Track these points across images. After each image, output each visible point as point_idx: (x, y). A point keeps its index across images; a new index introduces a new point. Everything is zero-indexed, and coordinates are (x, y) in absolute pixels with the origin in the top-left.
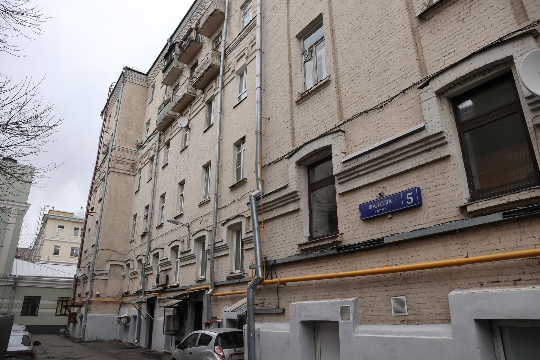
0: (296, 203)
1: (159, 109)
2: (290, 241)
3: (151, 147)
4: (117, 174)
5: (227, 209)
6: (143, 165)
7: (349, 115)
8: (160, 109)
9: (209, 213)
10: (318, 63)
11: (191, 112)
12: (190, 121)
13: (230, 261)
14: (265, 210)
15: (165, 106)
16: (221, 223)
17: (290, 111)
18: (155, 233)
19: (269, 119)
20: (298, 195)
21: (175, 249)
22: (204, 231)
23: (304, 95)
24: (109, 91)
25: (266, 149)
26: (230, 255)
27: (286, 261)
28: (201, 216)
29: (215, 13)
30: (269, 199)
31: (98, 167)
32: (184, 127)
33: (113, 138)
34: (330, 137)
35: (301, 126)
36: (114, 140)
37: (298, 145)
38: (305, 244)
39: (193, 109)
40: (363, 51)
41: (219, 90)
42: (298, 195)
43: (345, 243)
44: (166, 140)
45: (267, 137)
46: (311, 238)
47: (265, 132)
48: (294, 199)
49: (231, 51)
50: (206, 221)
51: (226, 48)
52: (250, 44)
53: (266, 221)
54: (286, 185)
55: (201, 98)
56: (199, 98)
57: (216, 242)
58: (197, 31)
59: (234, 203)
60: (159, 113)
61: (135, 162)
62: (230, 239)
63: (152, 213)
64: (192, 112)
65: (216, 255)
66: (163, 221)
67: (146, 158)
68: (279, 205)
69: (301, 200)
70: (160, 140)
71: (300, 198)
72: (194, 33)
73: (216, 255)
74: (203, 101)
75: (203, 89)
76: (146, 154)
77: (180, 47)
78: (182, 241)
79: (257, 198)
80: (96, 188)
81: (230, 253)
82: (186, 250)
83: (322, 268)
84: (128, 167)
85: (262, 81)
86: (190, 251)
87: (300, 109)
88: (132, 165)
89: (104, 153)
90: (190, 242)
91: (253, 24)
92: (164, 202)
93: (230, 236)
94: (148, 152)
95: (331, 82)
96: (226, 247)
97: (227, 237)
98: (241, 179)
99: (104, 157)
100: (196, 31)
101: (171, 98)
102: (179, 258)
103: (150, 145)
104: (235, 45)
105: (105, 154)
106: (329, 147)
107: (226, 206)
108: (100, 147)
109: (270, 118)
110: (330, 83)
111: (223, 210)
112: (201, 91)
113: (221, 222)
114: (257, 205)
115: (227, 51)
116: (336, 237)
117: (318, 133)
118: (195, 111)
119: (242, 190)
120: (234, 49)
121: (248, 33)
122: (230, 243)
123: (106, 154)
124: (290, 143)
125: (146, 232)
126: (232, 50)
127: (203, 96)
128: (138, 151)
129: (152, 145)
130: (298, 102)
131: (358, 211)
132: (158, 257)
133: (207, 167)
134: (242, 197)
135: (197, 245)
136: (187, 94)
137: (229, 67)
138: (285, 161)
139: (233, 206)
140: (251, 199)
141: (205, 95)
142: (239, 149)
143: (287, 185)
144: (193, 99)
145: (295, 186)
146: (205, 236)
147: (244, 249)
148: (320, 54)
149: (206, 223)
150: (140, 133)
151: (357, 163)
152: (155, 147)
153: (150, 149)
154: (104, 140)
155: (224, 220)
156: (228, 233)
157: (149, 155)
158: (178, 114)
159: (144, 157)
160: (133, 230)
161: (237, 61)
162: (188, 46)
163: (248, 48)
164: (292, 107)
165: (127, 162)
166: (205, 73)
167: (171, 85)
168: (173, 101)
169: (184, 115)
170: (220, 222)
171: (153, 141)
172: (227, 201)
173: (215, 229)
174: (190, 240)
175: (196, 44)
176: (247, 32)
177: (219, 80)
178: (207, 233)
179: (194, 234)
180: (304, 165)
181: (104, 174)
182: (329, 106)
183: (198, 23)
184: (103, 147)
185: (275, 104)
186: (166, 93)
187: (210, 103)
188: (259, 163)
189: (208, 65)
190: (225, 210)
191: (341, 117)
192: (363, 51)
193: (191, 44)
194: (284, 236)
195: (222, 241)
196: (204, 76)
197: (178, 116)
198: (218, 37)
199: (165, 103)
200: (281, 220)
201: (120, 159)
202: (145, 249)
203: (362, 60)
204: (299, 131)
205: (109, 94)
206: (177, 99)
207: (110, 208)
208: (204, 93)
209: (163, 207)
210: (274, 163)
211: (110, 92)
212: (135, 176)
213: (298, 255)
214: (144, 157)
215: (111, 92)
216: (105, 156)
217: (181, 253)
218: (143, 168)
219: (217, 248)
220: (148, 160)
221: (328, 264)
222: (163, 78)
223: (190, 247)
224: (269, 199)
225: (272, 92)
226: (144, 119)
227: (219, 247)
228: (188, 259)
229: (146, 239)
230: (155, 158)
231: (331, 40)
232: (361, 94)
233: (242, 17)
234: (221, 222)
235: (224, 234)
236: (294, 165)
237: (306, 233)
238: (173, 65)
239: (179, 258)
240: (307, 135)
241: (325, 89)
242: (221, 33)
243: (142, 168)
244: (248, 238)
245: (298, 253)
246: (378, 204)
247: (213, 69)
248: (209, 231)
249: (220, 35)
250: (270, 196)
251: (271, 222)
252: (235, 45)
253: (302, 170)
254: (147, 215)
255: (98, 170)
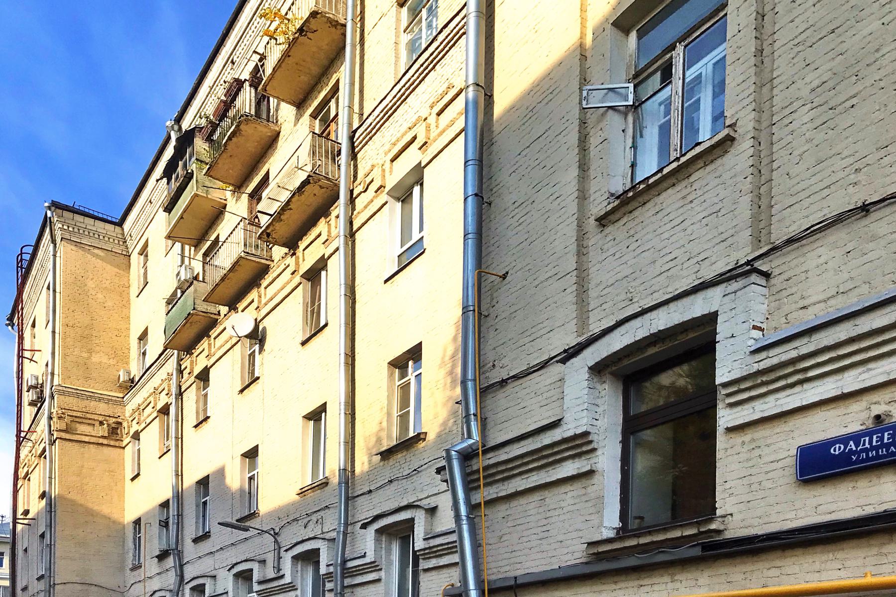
0: (583, 458)
1: (168, 303)
2: (560, 538)
3: (159, 387)
4: (76, 445)
5: (373, 496)
6: (143, 425)
7: (791, 229)
8: (171, 301)
9: (327, 506)
10: (688, 104)
11: (260, 302)
12: (260, 322)
13: (383, 591)
14: (489, 480)
15: (183, 293)
16: (360, 524)
17: (576, 247)
18: (190, 550)
19: (504, 277)
20: (591, 442)
21: (243, 575)
22: (316, 540)
23: (631, 194)
24: (18, 267)
25: (494, 349)
26: (383, 581)
27: (544, 578)
28: (307, 514)
29: (313, 24)
30: (503, 455)
31: (24, 431)
32: (246, 336)
33: (50, 371)
34: (718, 291)
35: (611, 281)
36: (53, 374)
37: (596, 328)
38: (609, 541)
39: (265, 294)
40: (885, 20)
41: (340, 242)
42: (591, 442)
43: (732, 533)
44: (197, 370)
45: (496, 321)
46: (623, 532)
47: (492, 310)
48: (579, 450)
49: (370, 136)
50: (319, 522)
51: (354, 128)
52: (432, 107)
53: (490, 503)
54: (555, 421)
55: (289, 266)
56: (282, 267)
57: (348, 558)
58: (256, 89)
59: (392, 485)
60: (170, 310)
61: (120, 420)
62: (383, 552)
63: (178, 515)
64: (264, 301)
65: (347, 582)
66: (209, 529)
67: (149, 410)
68: (531, 466)
69: (599, 452)
70: (180, 372)
71: (596, 447)
72: (246, 100)
73: (347, 582)
74: (293, 273)
75: (292, 245)
76: (148, 402)
77: (209, 139)
78: (260, 562)
79: (467, 456)
80: (27, 474)
81: (383, 577)
82: (271, 574)
83: (656, 587)
84: (103, 431)
85: (484, 180)
86: (282, 576)
87: (610, 237)
88: (114, 425)
89: (32, 404)
90: (281, 563)
91: (441, 43)
92: (206, 494)
93: (384, 546)
94: (151, 399)
95: (736, 142)
96: (373, 567)
97: (375, 547)
98: (411, 434)
99: (36, 411)
100: (253, 91)
101: (198, 274)
102: (254, 590)
103: (156, 382)
104: (384, 115)
105: (36, 405)
106: (711, 319)
107: (370, 491)
108: (20, 392)
109: (507, 273)
110: (731, 146)
111: (360, 500)
112: (286, 250)
113: (360, 521)
114: (465, 470)
115: (357, 135)
116: (711, 520)
117: (670, 289)
118: (271, 299)
119: (413, 458)
120: (379, 128)
121: (427, 74)
122: (383, 560)
123: (39, 405)
124: (572, 326)
125: (170, 550)
126: (375, 133)
127: (290, 261)
128: (125, 399)
129: (160, 382)
130: (603, 221)
131: (791, 461)
132: (203, 592)
133: (316, 415)
134: (415, 470)
135: (299, 566)
136: (243, 258)
137: (368, 180)
138: (556, 369)
139: (391, 489)
140: (449, 458)
141: (298, 258)
142: (403, 375)
143: (560, 420)
144: (264, 270)
145: (585, 421)
146: (319, 549)
147: (420, 568)
148: (696, 74)
149: (320, 526)
150: (125, 360)
151: (806, 346)
152: (169, 386)
153: (156, 392)
154: (27, 375)
155: (369, 518)
156: (377, 541)
157: (156, 404)
158: (224, 310)
159: (143, 410)
160: (136, 548)
161: (392, 161)
162: (234, 134)
163: (426, 119)
164: (581, 236)
165: (98, 420)
166: (293, 200)
167: (197, 245)
168: (207, 279)
169: (243, 311)
170: (356, 522)
171: (162, 374)
172: (374, 482)
173: (343, 535)
174: (281, 560)
175: (258, 127)
176: (422, 72)
177: (337, 217)
178: (323, 543)
179: (288, 547)
180: (612, 374)
181: (42, 445)
182: (720, 214)
183: (259, 64)
184: (28, 391)
185: (526, 236)
186: (183, 262)
187: (314, 275)
188: (471, 380)
189: (303, 176)
190: (370, 498)
191: (757, 240)
192: (885, 20)
193: (242, 127)
194: (545, 528)
195: (364, 556)
196: (291, 209)
197: (225, 315)
198: (325, 102)
199: (184, 286)
200: (536, 497)
201: (79, 414)
202: (171, 579)
203: (877, 50)
204: (602, 293)
205: (20, 274)
206: (214, 276)
207: (70, 510)
208: (294, 254)
209: (205, 503)
210: (516, 377)
211: (22, 268)
212: (124, 448)
213: (586, 563)
214: (143, 410)
215: (24, 270)
216: (36, 409)
217: (260, 583)
218: (142, 430)
219: (350, 570)
220: (155, 414)
221: (676, 578)
222: (169, 226)
223: (281, 572)
224: (503, 455)
225: (517, 204)
226: (128, 329)
227: (356, 567)
228: (277, 592)
229: (170, 561)
230: (172, 410)
231: (753, 8)
232: (851, 160)
233: (404, 32)
234: (360, 521)
235: (368, 543)
236: (585, 374)
237: (611, 520)
238: (191, 190)
239: (254, 590)
240: (631, 300)
241: (709, 168)
242: (336, 89)
243: (141, 432)
244: (430, 548)
245: (584, 560)
246: (864, 441)
247: (317, 187)
248: (328, 540)
249: (332, 97)
250: (507, 449)
251: (506, 503)
252: (384, 115)
253: (606, 386)
254: (166, 520)
255: (24, 438)
